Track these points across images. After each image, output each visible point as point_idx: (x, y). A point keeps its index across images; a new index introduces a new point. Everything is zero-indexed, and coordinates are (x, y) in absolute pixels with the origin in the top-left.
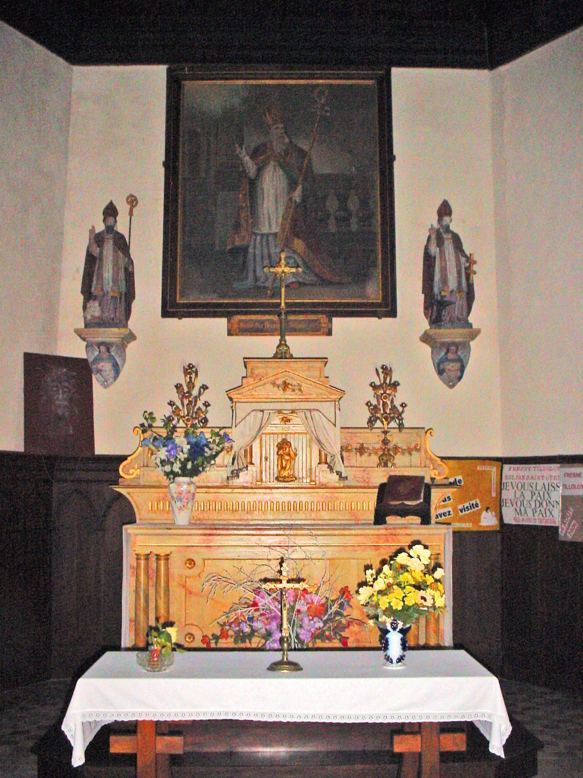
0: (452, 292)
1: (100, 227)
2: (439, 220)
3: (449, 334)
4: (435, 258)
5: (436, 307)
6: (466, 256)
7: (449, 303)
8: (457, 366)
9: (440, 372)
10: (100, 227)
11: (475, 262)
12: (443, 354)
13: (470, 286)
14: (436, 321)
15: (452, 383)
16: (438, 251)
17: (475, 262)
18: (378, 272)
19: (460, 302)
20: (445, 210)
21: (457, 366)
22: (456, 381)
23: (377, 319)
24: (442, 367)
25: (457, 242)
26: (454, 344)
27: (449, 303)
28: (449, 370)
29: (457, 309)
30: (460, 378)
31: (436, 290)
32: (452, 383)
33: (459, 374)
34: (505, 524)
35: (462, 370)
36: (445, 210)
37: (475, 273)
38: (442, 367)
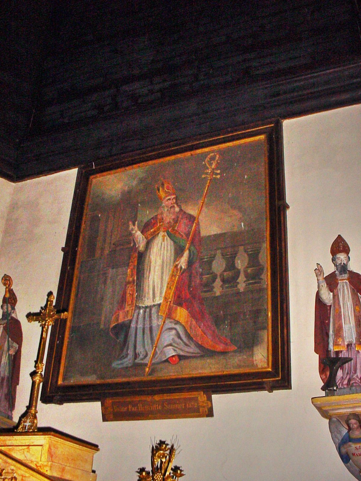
0: (349, 345)
12: (345, 431)
16: (332, 297)
20: (340, 247)
28: (354, 454)
38: (343, 450)
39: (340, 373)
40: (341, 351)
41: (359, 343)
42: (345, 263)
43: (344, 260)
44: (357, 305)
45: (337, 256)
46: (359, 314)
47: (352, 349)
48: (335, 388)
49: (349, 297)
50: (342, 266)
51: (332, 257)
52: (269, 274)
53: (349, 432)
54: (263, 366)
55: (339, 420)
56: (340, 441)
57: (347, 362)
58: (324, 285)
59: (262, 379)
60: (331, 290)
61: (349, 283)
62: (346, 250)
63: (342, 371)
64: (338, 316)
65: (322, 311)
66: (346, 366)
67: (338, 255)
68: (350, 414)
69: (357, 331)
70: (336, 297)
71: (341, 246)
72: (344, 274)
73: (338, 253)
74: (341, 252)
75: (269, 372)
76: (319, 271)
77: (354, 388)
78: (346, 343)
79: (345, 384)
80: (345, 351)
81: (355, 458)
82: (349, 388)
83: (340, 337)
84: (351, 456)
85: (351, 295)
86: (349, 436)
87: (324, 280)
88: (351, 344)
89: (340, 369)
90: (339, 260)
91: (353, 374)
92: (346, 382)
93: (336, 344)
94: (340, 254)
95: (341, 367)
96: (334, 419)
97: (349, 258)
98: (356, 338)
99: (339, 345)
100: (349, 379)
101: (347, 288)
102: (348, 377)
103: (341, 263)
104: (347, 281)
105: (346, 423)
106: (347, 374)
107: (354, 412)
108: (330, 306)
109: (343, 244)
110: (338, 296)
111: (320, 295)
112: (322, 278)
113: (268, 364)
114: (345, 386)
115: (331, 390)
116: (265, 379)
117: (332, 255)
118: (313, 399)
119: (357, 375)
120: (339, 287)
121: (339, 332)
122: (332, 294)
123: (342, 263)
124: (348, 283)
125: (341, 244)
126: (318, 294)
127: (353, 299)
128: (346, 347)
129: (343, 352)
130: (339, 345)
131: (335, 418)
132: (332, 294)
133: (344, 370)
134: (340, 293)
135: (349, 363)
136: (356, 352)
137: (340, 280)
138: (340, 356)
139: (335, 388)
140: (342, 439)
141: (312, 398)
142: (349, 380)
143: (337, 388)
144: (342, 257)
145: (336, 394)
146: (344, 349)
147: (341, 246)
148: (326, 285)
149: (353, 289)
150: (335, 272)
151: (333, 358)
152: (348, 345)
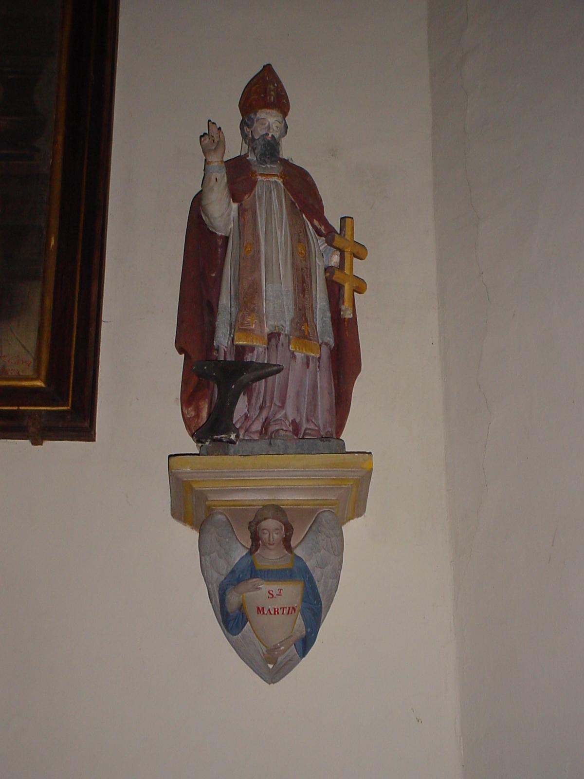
0: (273, 336)
1: (235, 147)
2: (243, 124)
3: (261, 477)
4: (226, 239)
5: (217, 387)
6: (328, 234)
7: (267, 371)
8: (290, 593)
9: (232, 620)
10: (235, 147)
11: (360, 252)
12: (239, 553)
13: (345, 331)
14: (213, 430)
15: (273, 666)
16: (234, 213)
17: (360, 252)
18: (37, 298)
19: (301, 375)
20: (264, 93)
21: (290, 593)
22: (293, 650)
23: (27, 443)
24: (233, 599)
25: (303, 193)
26: (278, 511)
27: (267, 371)
28: (260, 610)
29: (301, 375)
30: (305, 644)
31: (223, 339)
32: (273, 666)
33: (300, 626)
34: (193, 525)
35: (313, 609)
36: (264, 93)
37: (360, 287)
38: (233, 599)
39: (241, 406)
40: (252, 349)
41: (297, 333)
42: (277, 136)
43: (275, 128)
44: (299, 241)
45: (258, 115)
46: (304, 262)
47: (280, 348)
48: (233, 437)
49: (282, 218)
50: (269, 141)
51: (240, 118)
52: (60, 138)
53: (252, 552)
54: (21, 374)
55: (229, 521)
56: (223, 578)
57: (265, 376)
58: (220, 177)
59: (19, 406)
60: (235, 195)
61: (284, 184)
62: (282, 105)
63: (246, 398)
64: (250, 262)
65: (203, 251)
66: (260, 386)
67: (262, 114)
68: (265, 507)
69: (295, 304)
70: (249, 216)
71: (272, 93)
72: (270, 164)
73: (261, 108)
74: (268, 106)
75: (37, 390)
76: (211, 139)
77: (278, 442)
78: (267, 330)
79: (257, 432)
80: (261, 349)
81: (263, 619)
82: (268, 441)
83: (253, 310)
84: (251, 612)
85: (288, 214)
86: (252, 564)
87: (223, 164)
88: (279, 334)
89: (244, 394)
90: (263, 127)
91: (277, 408)
92: (257, 426)
93: (236, 326)
94: (268, 111)
95: (247, 388)
96: (220, 516)
97: (286, 127)
98: (292, 321)
99: (247, 331)
100: (266, 419)
101: (279, 197)
102: (264, 415)
103: (267, 134)
104: (280, 181)
105: (249, 528)
106: (261, 408)
107: (273, 503)
108: (226, 239)
109: (277, 87)
110: (255, 213)
111: (204, 203)
112: (219, 160)
113: (37, 370)
114: (256, 437)
115: (221, 440)
116: (22, 406)
117: (242, 115)
118: (173, 459)
119: (286, 414)
120: (258, 189)
121: (248, 299)
122: (235, 206)
123: (270, 135)
124: (282, 185)
125: (272, 87)
126: (198, 204)
127: (292, 225)
128: (266, 338)
129: (255, 352)
130: (247, 331)
131: (221, 513)
132: (235, 206)
133: (255, 395)
134: (260, 205)
135: (270, 379)
136: (288, 354)
137: (262, 175)
138: (249, 358)
139: (233, 437)
140: (233, 572)
141: (170, 456)
142: (266, 424)
143: (237, 436)
144: (269, 119)
145: (232, 451)
146: (261, 347)
147: (272, 93)
148: (225, 180)
149: (293, 203)
150: (246, 155)
151: (231, 361)
152: (271, 336)
